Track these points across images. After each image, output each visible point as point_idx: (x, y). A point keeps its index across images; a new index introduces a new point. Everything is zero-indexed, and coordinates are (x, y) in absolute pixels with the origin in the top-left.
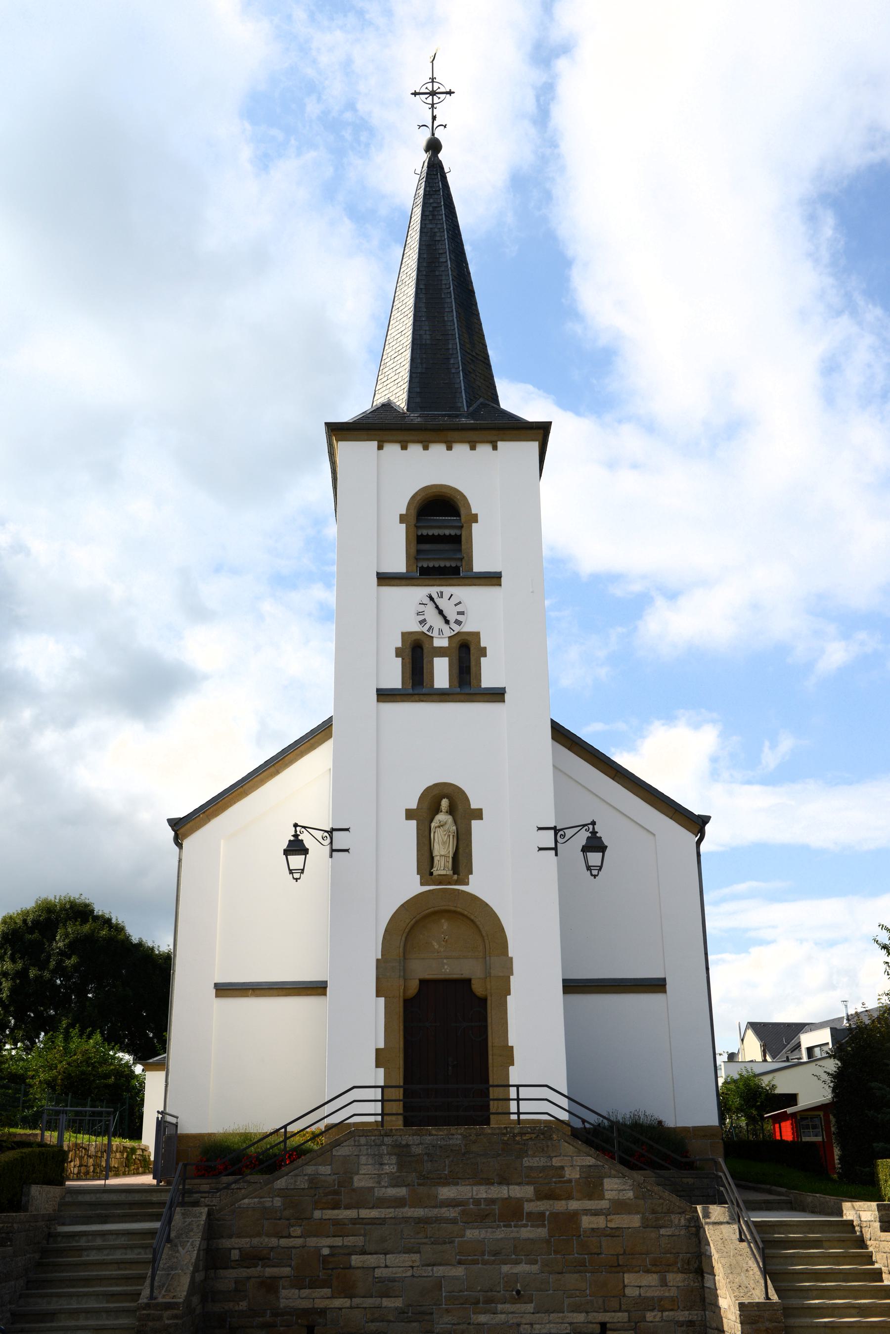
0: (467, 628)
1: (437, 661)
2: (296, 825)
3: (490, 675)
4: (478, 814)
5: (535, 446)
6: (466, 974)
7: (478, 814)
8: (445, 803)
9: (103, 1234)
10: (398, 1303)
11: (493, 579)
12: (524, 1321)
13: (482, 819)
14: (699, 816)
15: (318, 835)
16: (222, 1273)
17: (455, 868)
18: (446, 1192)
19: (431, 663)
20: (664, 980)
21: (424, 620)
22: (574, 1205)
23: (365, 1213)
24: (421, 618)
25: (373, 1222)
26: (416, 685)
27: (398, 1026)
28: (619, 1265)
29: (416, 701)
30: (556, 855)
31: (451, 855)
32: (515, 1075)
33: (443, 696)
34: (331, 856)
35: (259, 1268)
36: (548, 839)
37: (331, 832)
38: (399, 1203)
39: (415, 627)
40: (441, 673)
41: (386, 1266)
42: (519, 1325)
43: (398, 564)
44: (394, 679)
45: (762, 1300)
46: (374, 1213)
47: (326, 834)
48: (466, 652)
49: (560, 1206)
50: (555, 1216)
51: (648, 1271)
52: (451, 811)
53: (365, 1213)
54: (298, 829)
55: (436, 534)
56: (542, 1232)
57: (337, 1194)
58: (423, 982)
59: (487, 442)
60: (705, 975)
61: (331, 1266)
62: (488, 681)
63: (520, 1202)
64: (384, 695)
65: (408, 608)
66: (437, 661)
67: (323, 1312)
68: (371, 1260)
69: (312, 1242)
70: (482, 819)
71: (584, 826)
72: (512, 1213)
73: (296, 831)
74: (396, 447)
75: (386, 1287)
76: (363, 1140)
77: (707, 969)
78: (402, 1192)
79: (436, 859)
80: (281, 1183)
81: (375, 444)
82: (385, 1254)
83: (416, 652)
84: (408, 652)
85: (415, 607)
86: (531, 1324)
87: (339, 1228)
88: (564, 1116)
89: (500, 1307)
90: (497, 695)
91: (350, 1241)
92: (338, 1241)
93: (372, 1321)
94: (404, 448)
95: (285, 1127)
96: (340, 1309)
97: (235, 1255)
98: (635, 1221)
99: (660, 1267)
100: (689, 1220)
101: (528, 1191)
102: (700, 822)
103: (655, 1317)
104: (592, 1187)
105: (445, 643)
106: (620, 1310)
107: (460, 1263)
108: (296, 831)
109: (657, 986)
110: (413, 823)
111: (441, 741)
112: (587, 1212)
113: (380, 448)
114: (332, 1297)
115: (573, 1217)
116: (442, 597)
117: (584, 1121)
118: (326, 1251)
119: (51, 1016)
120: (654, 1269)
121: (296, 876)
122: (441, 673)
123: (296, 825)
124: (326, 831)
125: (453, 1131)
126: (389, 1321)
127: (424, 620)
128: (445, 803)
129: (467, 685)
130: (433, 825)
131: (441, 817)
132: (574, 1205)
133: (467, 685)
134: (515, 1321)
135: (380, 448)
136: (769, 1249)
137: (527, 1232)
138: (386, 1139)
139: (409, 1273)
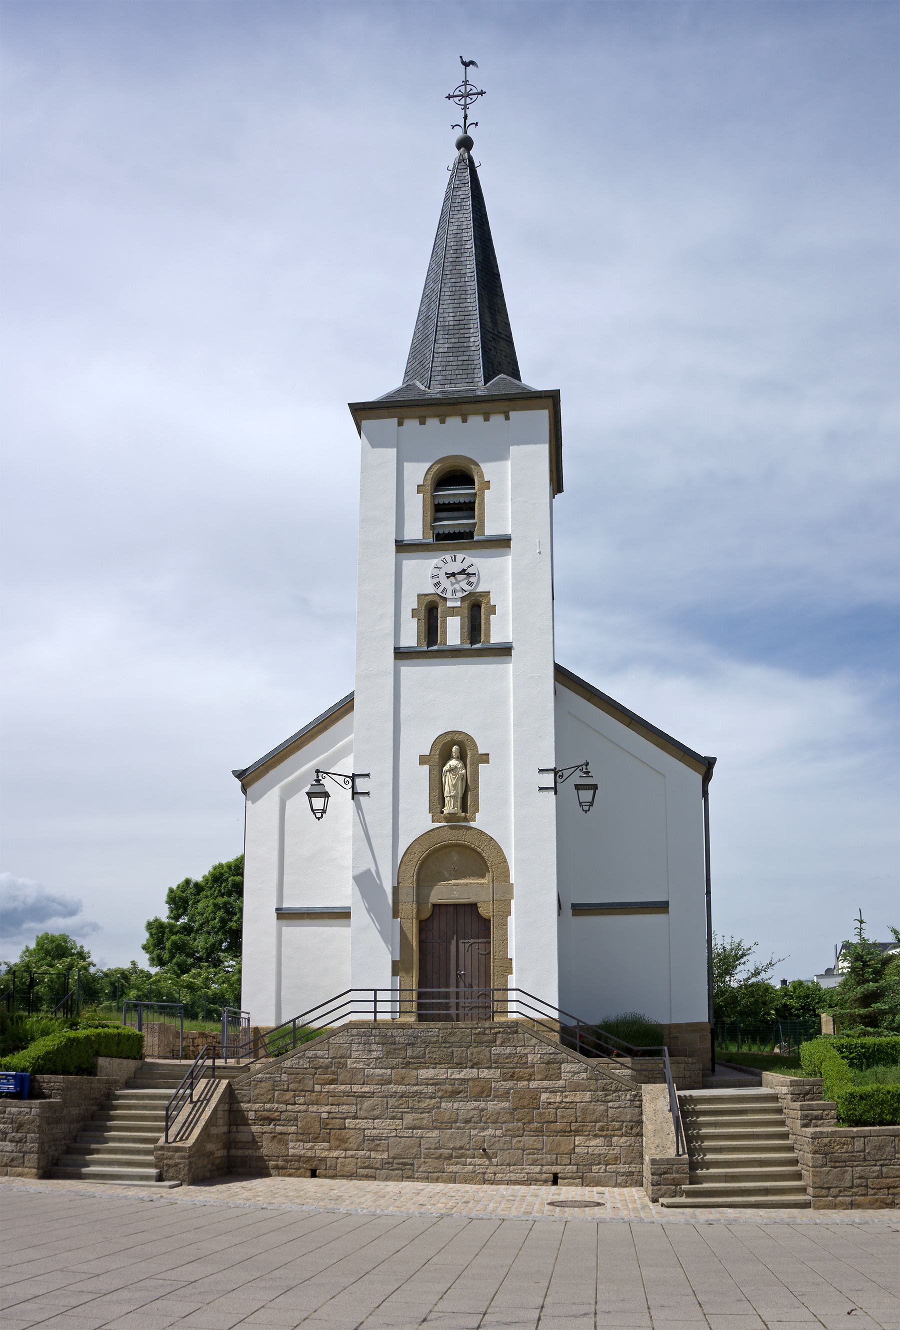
0: (481, 589)
1: (450, 620)
2: (318, 771)
3: (499, 631)
4: (485, 758)
5: (543, 416)
6: (473, 899)
7: (485, 758)
9: (143, 1097)
11: (503, 543)
12: (488, 1171)
13: (488, 763)
14: (705, 758)
15: (340, 780)
16: (242, 1128)
17: (464, 808)
18: (426, 1073)
19: (444, 623)
20: (667, 903)
21: (439, 583)
22: (533, 1085)
24: (436, 581)
26: (431, 646)
28: (571, 1131)
29: (430, 658)
30: (556, 793)
31: (460, 795)
32: (513, 981)
33: (455, 653)
34: (353, 798)
35: (271, 1126)
36: (548, 780)
37: (353, 777)
39: (431, 590)
40: (453, 631)
41: (374, 1128)
42: (484, 1173)
43: (415, 531)
44: (410, 638)
45: (673, 1156)
47: (347, 779)
48: (476, 610)
51: (596, 1136)
52: (462, 757)
54: (320, 774)
55: (452, 502)
57: (333, 1071)
58: (434, 906)
59: (500, 413)
60: (286, 878)
61: (329, 1127)
63: (488, 1081)
65: (424, 574)
66: (450, 620)
67: (324, 1160)
68: (362, 1123)
70: (488, 763)
71: (578, 767)
72: (484, 1092)
73: (318, 777)
74: (415, 423)
76: (355, 1031)
77: (708, 893)
79: (447, 800)
80: (288, 1063)
81: (395, 420)
82: (374, 1119)
83: (430, 614)
84: (423, 613)
85: (430, 571)
86: (495, 1174)
87: (337, 1099)
88: (555, 1015)
89: (469, 1160)
92: (335, 1109)
93: (363, 1168)
94: (423, 423)
95: (294, 1020)
96: (337, 1158)
97: (251, 1115)
99: (606, 1133)
100: (635, 1096)
101: (495, 1073)
102: (709, 763)
103: (600, 1169)
104: (551, 1069)
106: (570, 1164)
107: (435, 1128)
108: (318, 777)
109: (662, 907)
110: (426, 768)
111: (448, 695)
112: (546, 1089)
113: (400, 424)
114: (330, 1149)
116: (455, 560)
117: (579, 1021)
118: (324, 1115)
119: (776, 1055)
120: (600, 1133)
121: (586, 808)
122: (453, 631)
123: (318, 771)
124: (349, 777)
125: (432, 1026)
126: (377, 1169)
127: (439, 583)
129: (478, 645)
130: (446, 768)
131: (453, 763)
132: (533, 1085)
133: (478, 645)
134: (481, 1171)
135: (400, 424)
136: (685, 1116)
137: (492, 1106)
138: (374, 1031)
139: (394, 1134)
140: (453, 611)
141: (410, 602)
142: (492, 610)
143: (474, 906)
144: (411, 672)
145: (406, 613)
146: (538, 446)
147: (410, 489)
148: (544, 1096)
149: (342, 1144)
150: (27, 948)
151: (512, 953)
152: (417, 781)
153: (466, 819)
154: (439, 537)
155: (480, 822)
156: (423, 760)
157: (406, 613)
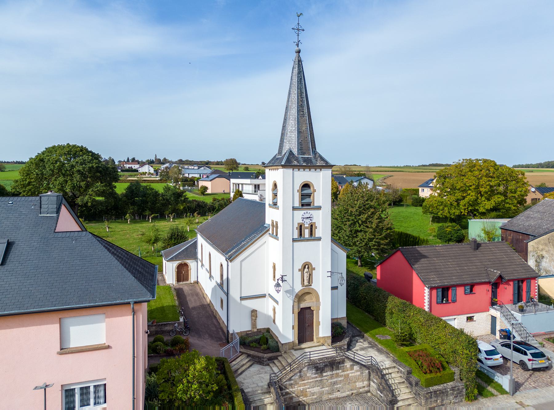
3: (318, 233)
4: (314, 269)
7: (314, 269)
8: (307, 266)
10: (316, 397)
11: (319, 208)
19: (304, 231)
23: (309, 381)
25: (311, 382)
27: (297, 320)
33: (308, 240)
36: (329, 274)
38: (316, 377)
40: (307, 233)
43: (297, 204)
44: (296, 236)
46: (311, 380)
48: (312, 228)
49: (346, 373)
50: (345, 375)
53: (309, 381)
56: (342, 378)
62: (317, 236)
64: (294, 240)
65: (299, 215)
69: (299, 388)
75: (313, 394)
78: (316, 375)
83: (301, 228)
85: (301, 216)
90: (319, 239)
91: (306, 387)
98: (359, 373)
105: (308, 226)
115: (348, 375)
122: (307, 233)
128: (307, 266)
129: (312, 237)
132: (348, 372)
140: (307, 228)
141: (296, 225)
142: (316, 228)
143: (310, 307)
144: (299, 245)
145: (295, 228)
146: (105, 338)
147: (296, 191)
148: (350, 375)
149: (306, 396)
150: (216, 282)
151: (320, 320)
152: (298, 275)
153: (310, 285)
154: (302, 205)
155: (313, 286)
156: (299, 270)
157: (295, 228)
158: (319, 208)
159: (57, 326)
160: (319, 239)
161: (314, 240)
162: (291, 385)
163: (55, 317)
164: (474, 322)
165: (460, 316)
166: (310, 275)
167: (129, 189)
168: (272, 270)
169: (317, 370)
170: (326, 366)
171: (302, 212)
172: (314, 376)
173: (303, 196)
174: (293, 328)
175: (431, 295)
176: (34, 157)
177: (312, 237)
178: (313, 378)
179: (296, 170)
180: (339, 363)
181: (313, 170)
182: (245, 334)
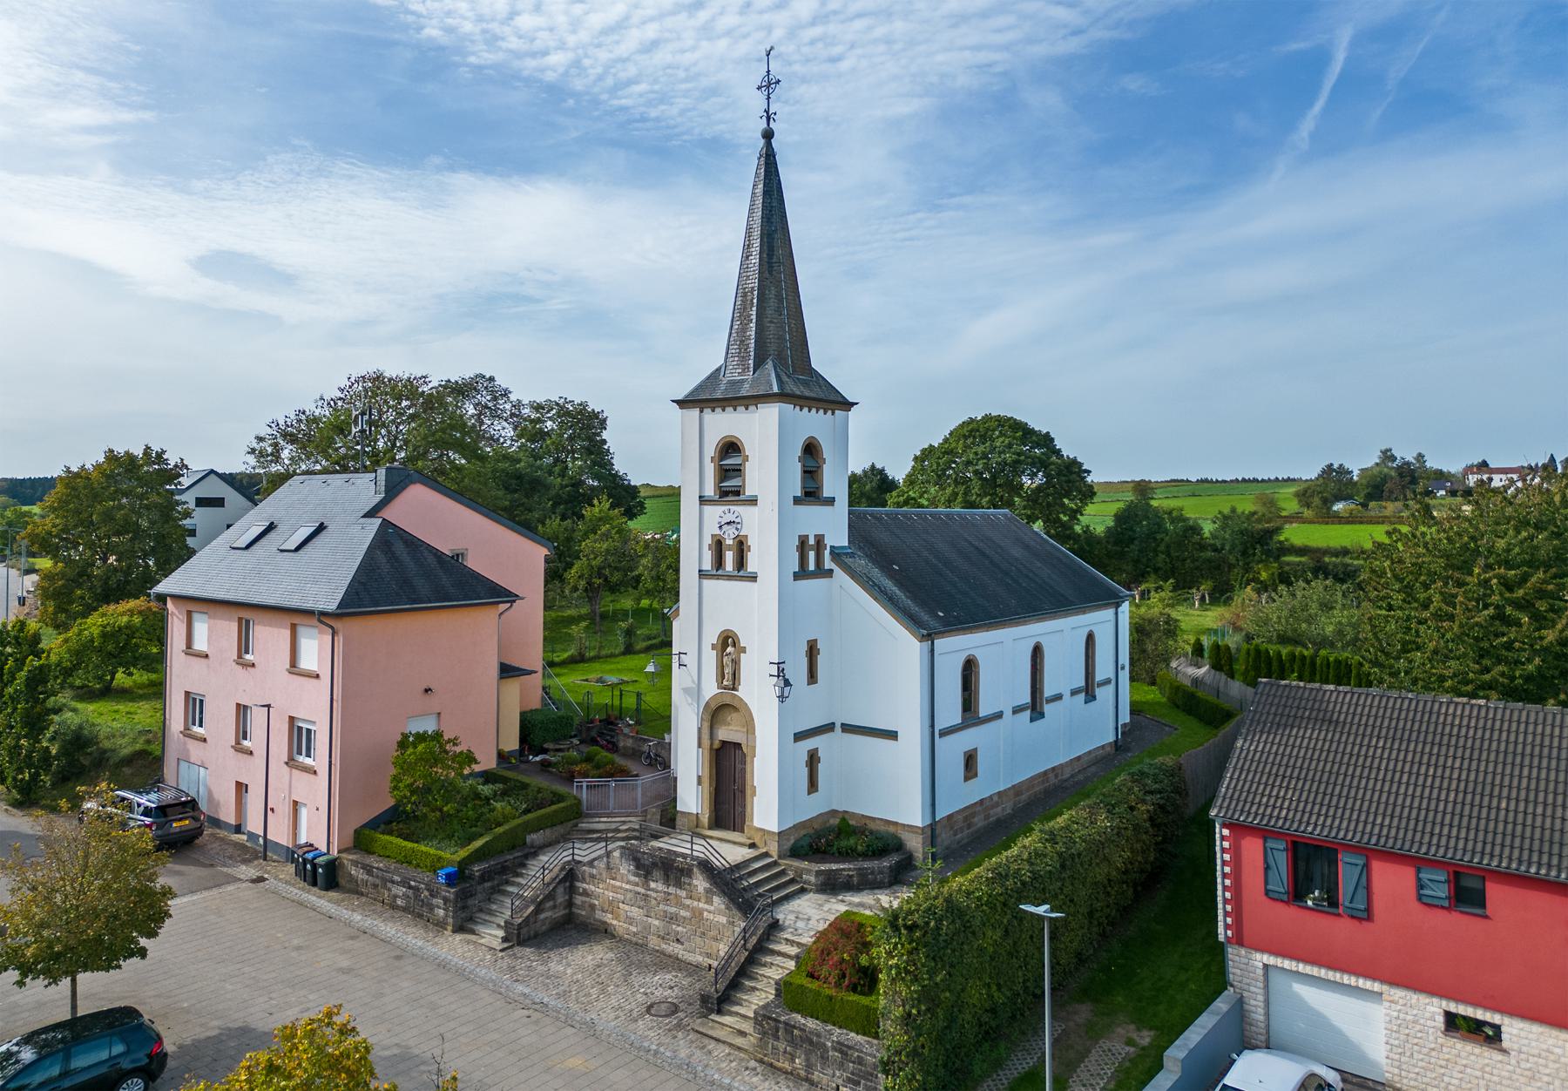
33: (730, 577)
43: (710, 491)
44: (707, 565)
48: (741, 547)
50: (693, 910)
65: (715, 513)
83: (718, 546)
90: (753, 578)
141: (708, 540)
145: (706, 548)
152: (710, 658)
153: (734, 689)
155: (741, 692)
157: (706, 548)
158: (753, 501)
159: (287, 633)
160: (753, 578)
161: (742, 578)
162: (592, 876)
163: (288, 620)
164: (1497, 1056)
165: (1398, 994)
166: (736, 663)
167: (1121, 518)
168: (805, 661)
169: (637, 867)
170: (654, 865)
171: (719, 509)
172: (633, 878)
173: (725, 473)
174: (699, 783)
175: (1236, 851)
176: (605, 435)
177: (741, 570)
178: (628, 882)
179: (707, 411)
180: (682, 871)
181: (718, 410)
182: (835, 821)
